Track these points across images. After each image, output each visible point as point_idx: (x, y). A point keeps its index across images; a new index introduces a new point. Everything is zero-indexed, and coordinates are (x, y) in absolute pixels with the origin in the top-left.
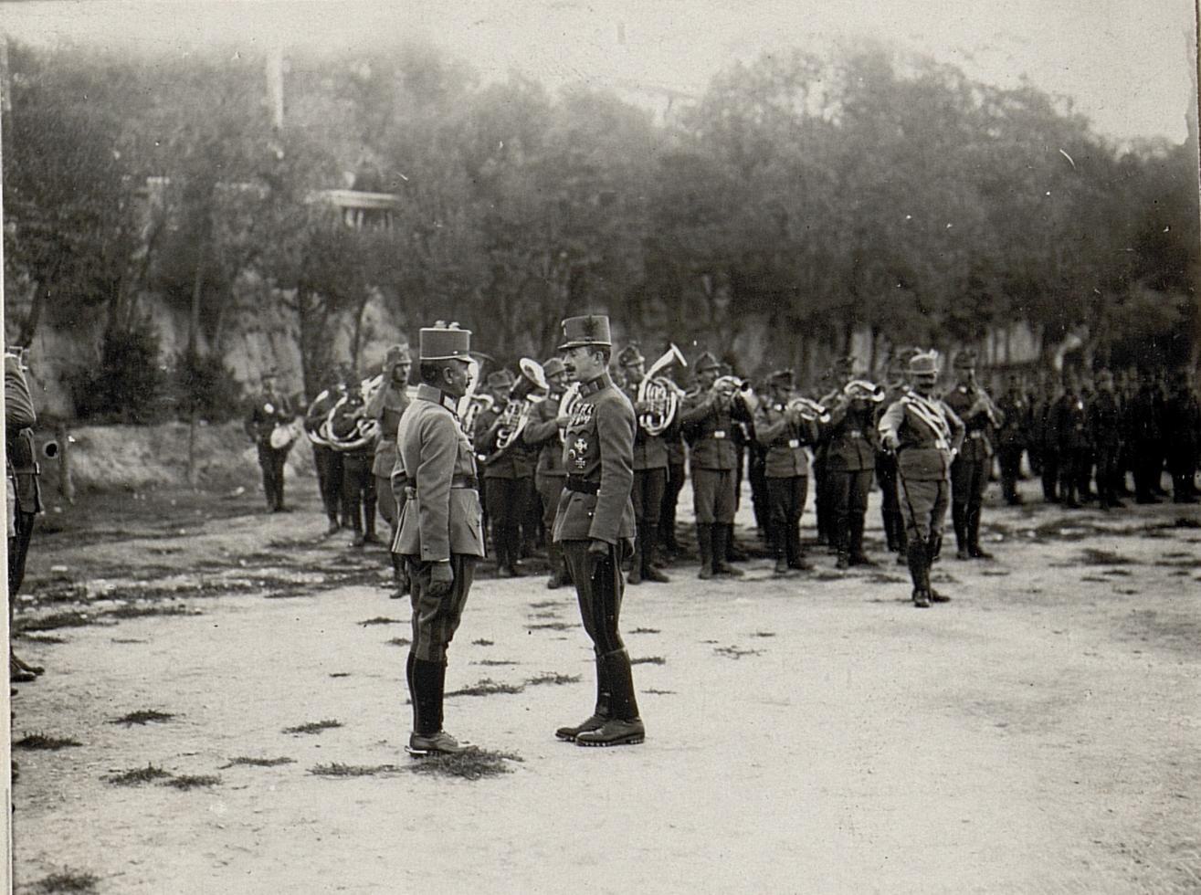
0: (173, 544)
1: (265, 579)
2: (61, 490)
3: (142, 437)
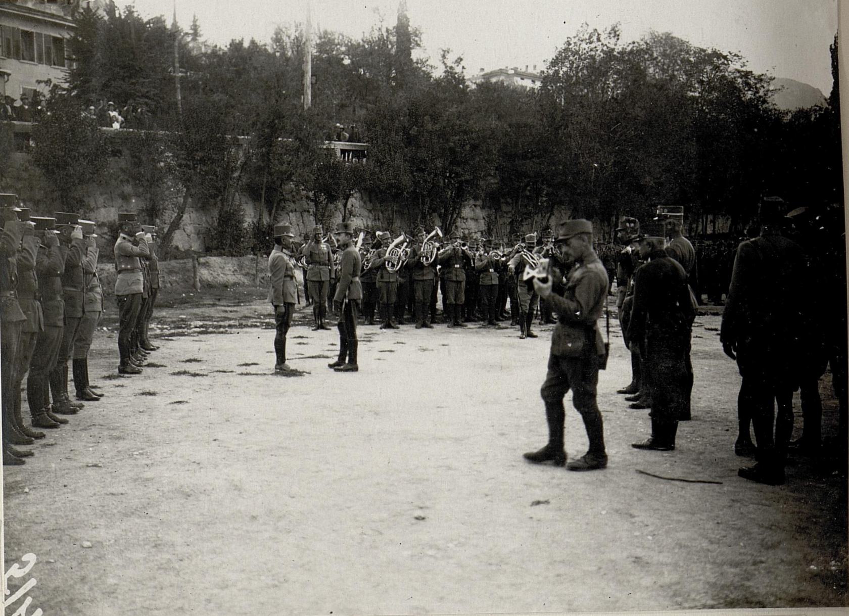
0: (235, 309)
1: (266, 323)
2: (194, 286)
3: (234, 262)
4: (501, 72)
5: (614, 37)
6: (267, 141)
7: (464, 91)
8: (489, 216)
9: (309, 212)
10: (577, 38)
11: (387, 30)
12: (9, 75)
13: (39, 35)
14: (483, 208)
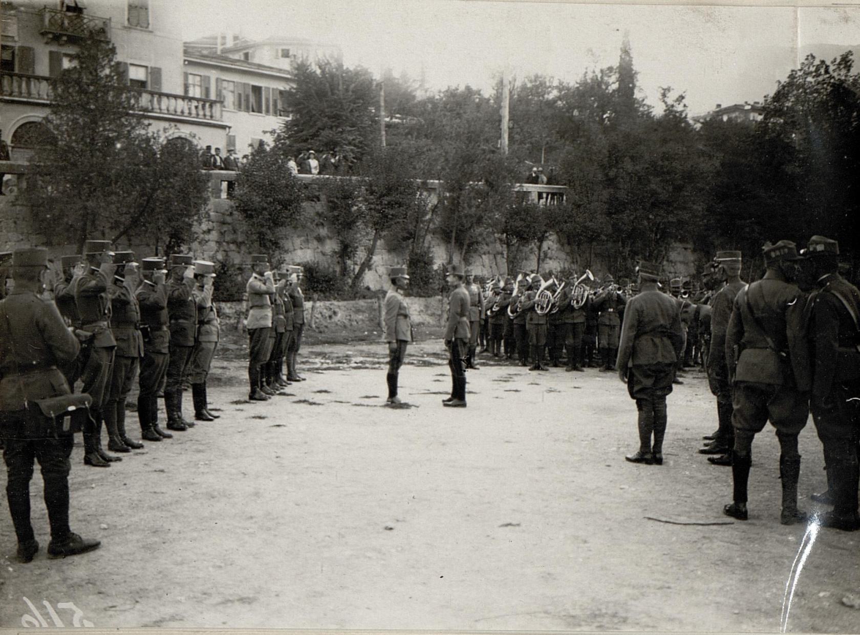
3: (421, 302)
4: (736, 108)
5: (844, 68)
6: (456, 187)
7: (688, 129)
8: (700, 260)
9: (502, 254)
10: (802, 72)
11: (602, 71)
12: (230, 128)
13: (267, 89)
14: (694, 251)
